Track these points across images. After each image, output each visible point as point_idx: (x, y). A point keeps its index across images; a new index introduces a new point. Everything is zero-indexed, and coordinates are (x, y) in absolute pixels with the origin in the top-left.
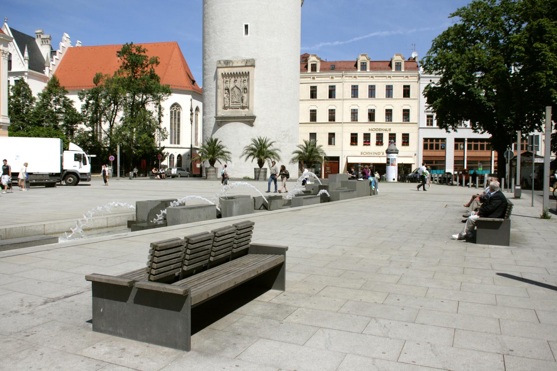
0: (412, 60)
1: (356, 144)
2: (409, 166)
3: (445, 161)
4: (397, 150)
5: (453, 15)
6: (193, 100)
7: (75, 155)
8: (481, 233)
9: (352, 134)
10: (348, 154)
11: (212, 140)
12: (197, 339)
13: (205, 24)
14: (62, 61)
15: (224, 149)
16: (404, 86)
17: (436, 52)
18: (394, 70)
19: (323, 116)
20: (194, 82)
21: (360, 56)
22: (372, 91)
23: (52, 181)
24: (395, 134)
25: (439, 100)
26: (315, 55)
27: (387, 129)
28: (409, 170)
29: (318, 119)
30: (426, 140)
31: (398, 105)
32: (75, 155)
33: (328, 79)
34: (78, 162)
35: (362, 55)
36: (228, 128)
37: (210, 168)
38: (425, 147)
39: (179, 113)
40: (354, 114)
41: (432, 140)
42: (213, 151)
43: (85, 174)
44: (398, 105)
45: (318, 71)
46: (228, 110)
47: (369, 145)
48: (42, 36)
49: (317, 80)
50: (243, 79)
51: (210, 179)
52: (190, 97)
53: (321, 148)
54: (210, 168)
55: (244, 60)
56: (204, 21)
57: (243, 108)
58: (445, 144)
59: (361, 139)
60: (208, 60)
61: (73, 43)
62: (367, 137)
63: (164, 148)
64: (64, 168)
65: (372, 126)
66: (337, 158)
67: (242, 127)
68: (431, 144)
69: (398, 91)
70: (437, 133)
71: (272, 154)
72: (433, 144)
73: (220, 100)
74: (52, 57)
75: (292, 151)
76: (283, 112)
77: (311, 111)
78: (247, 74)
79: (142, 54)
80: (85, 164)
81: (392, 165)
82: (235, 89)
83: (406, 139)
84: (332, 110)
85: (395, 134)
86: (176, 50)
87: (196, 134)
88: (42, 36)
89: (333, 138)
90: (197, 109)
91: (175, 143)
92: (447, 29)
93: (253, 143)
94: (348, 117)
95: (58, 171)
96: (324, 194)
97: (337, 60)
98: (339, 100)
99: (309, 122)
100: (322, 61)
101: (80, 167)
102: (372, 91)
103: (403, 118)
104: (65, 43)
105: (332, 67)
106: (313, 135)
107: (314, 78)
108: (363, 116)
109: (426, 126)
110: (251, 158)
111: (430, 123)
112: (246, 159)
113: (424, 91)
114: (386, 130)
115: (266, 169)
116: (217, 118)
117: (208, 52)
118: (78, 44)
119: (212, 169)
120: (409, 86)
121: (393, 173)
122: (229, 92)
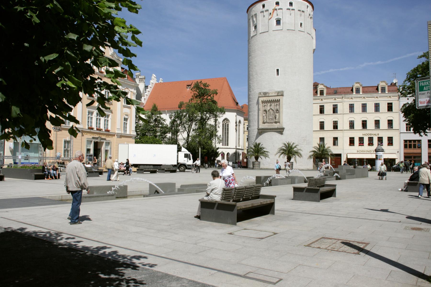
0: (394, 85)
1: (354, 145)
2: (394, 160)
3: (421, 156)
4: (383, 149)
5: (421, 57)
6: (237, 116)
7: (185, 154)
8: (410, 187)
9: (350, 138)
10: (348, 152)
11: (256, 144)
12: (321, 201)
13: (250, 69)
14: (152, 92)
15: (264, 150)
16: (388, 104)
17: (410, 81)
18: (380, 93)
19: (329, 126)
20: (237, 103)
21: (355, 84)
22: (364, 107)
23: (174, 169)
24: (382, 138)
25: (412, 115)
26: (322, 84)
27: (376, 134)
28: (394, 163)
29: (326, 128)
30: (405, 141)
31: (384, 117)
32: (185, 154)
33: (332, 100)
34: (186, 158)
35: (356, 83)
36: (266, 136)
37: (255, 162)
38: (405, 146)
39: (228, 125)
40: (352, 125)
41: (410, 141)
42: (258, 151)
43: (190, 165)
44: (384, 117)
45: (325, 95)
46: (266, 124)
47: (363, 145)
48: (140, 77)
49: (324, 101)
50: (276, 104)
51: (255, 169)
52: (235, 114)
53: (330, 148)
54: (255, 162)
55: (276, 92)
56: (249, 68)
57: (276, 122)
58: (421, 144)
59: (357, 141)
60: (252, 92)
61: (158, 80)
62: (361, 140)
63: (218, 148)
64: (179, 162)
65: (365, 132)
66: (340, 155)
67: (276, 135)
68: (408, 144)
69: (384, 107)
70: (413, 136)
71: (297, 153)
72: (411, 144)
73: (261, 118)
74: (145, 90)
75: (309, 151)
76: (302, 124)
77: (320, 122)
78: (278, 101)
79: (207, 88)
80: (190, 159)
81: (380, 159)
82: (271, 110)
83: (390, 141)
84: (335, 121)
85: (382, 138)
86: (226, 83)
87: (239, 139)
88: (140, 77)
89: (336, 141)
90: (240, 122)
91: (225, 145)
92: (417, 66)
93: (284, 145)
94: (347, 126)
95: (176, 164)
96: (337, 176)
97: (338, 87)
98: (340, 114)
99: (319, 130)
100: (327, 88)
101: (188, 161)
102: (364, 107)
103: (388, 126)
104: (153, 81)
105: (335, 92)
106: (322, 139)
107: (322, 100)
108: (358, 125)
109: (405, 132)
110: (282, 155)
111: (408, 129)
112: (280, 156)
113: (402, 109)
114: (375, 135)
115: (292, 163)
116: (259, 129)
117: (252, 87)
118: (161, 81)
119: (256, 163)
120: (391, 104)
121: (380, 166)
122: (266, 112)
